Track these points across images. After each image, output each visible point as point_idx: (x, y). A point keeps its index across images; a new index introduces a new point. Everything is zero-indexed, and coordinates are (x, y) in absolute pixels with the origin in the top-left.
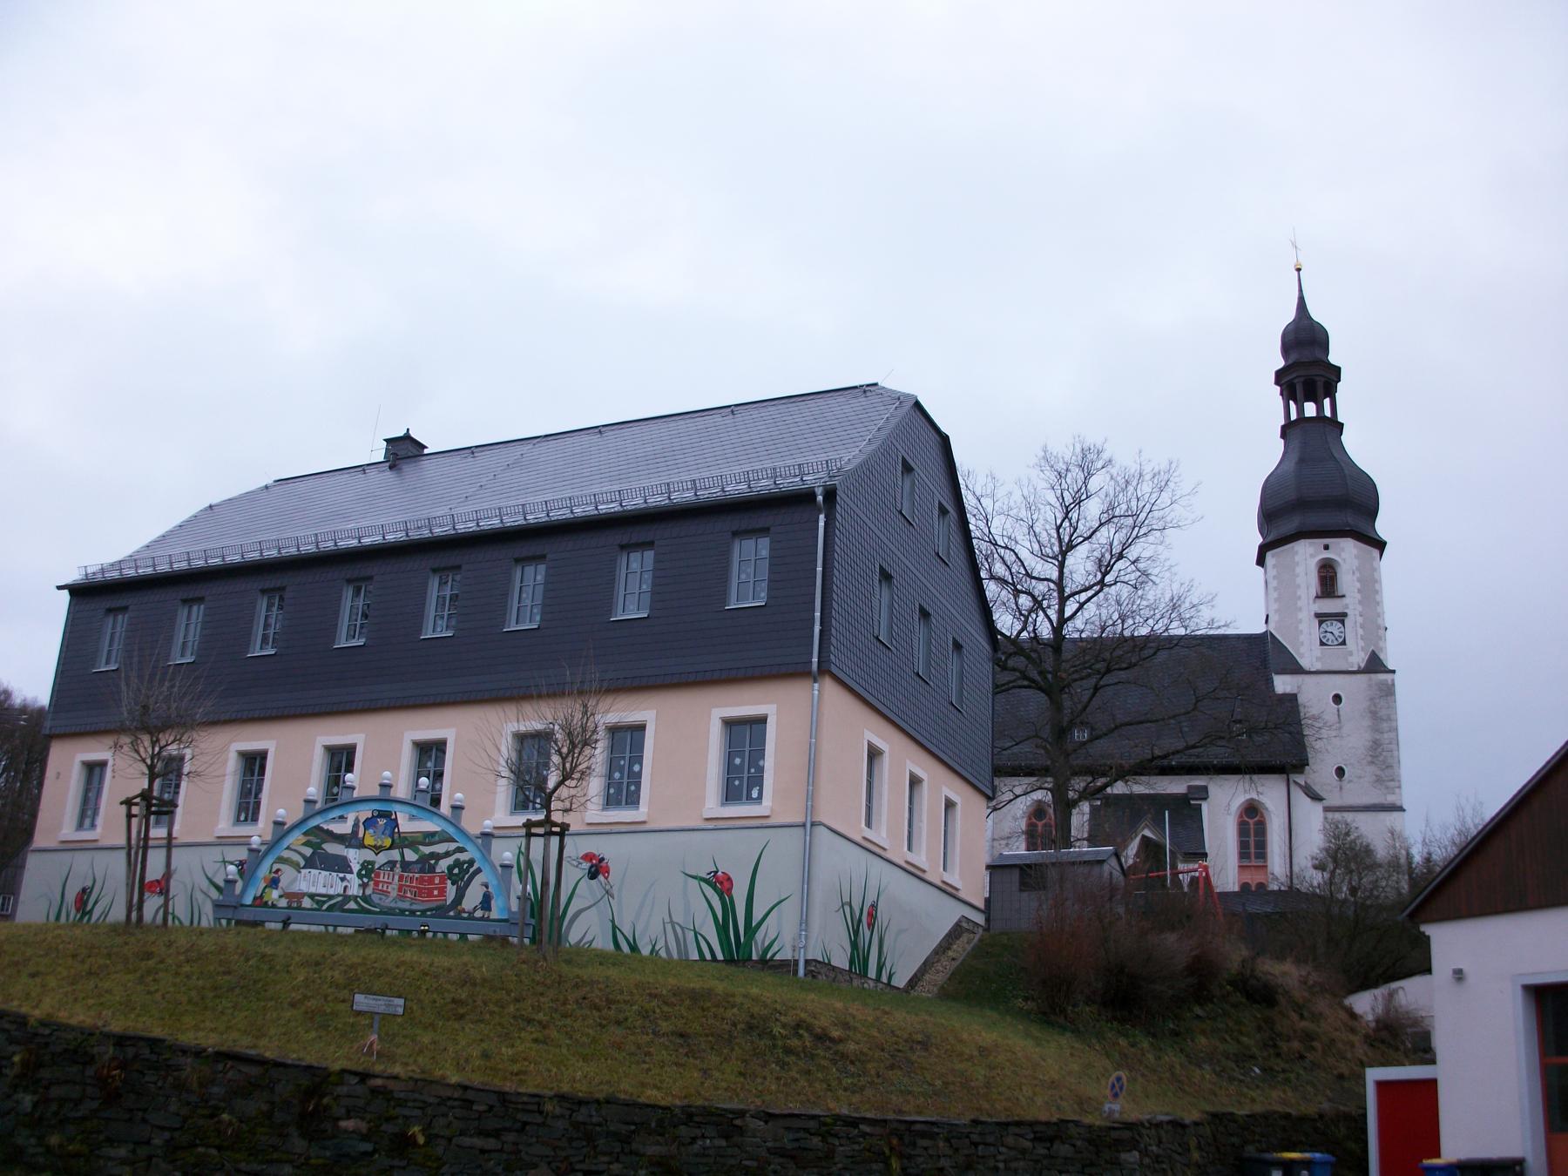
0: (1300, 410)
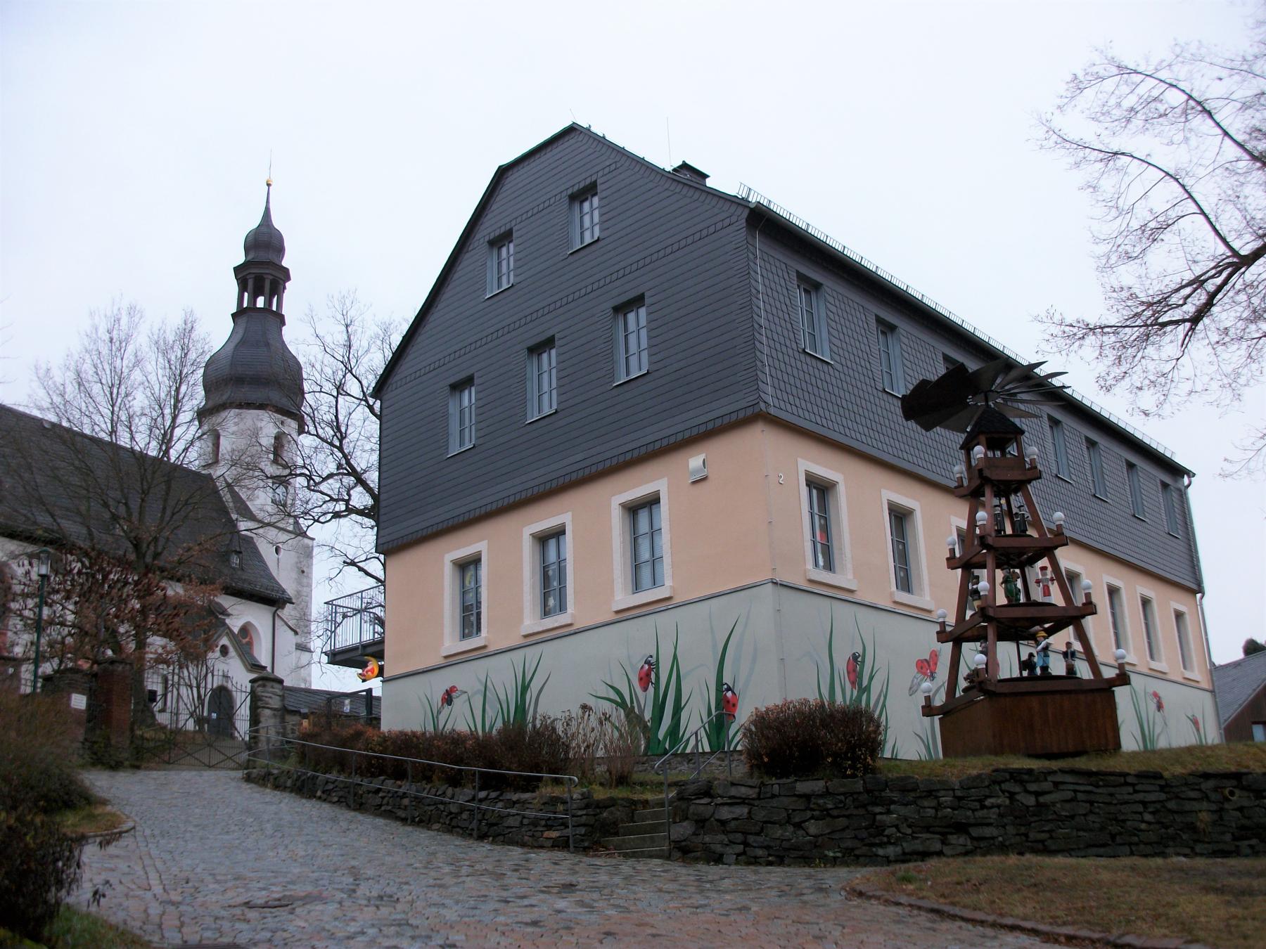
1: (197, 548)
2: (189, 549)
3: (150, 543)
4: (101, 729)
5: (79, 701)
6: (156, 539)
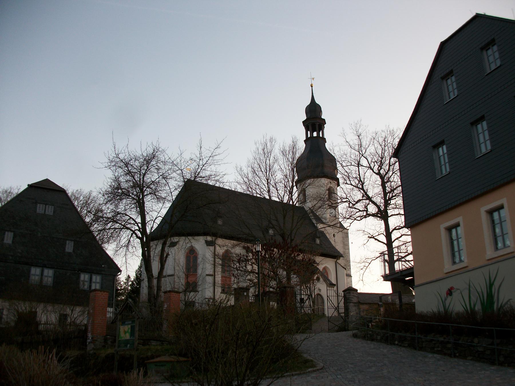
0: (312, 134)
6: (291, 234)
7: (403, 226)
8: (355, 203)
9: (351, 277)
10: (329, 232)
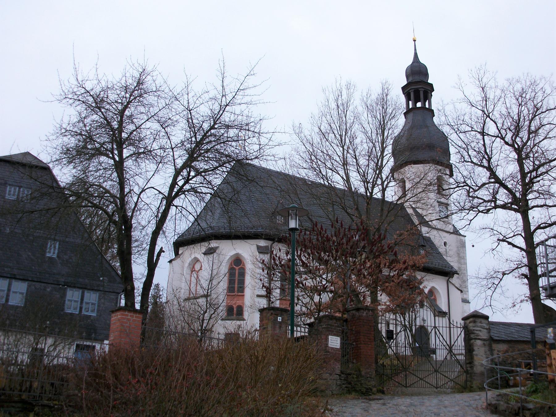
1: (406, 233)
2: (401, 235)
3: (375, 233)
4: (353, 363)
5: (334, 342)
7: (551, 223)
8: (477, 188)
9: (467, 304)
10: (437, 238)
